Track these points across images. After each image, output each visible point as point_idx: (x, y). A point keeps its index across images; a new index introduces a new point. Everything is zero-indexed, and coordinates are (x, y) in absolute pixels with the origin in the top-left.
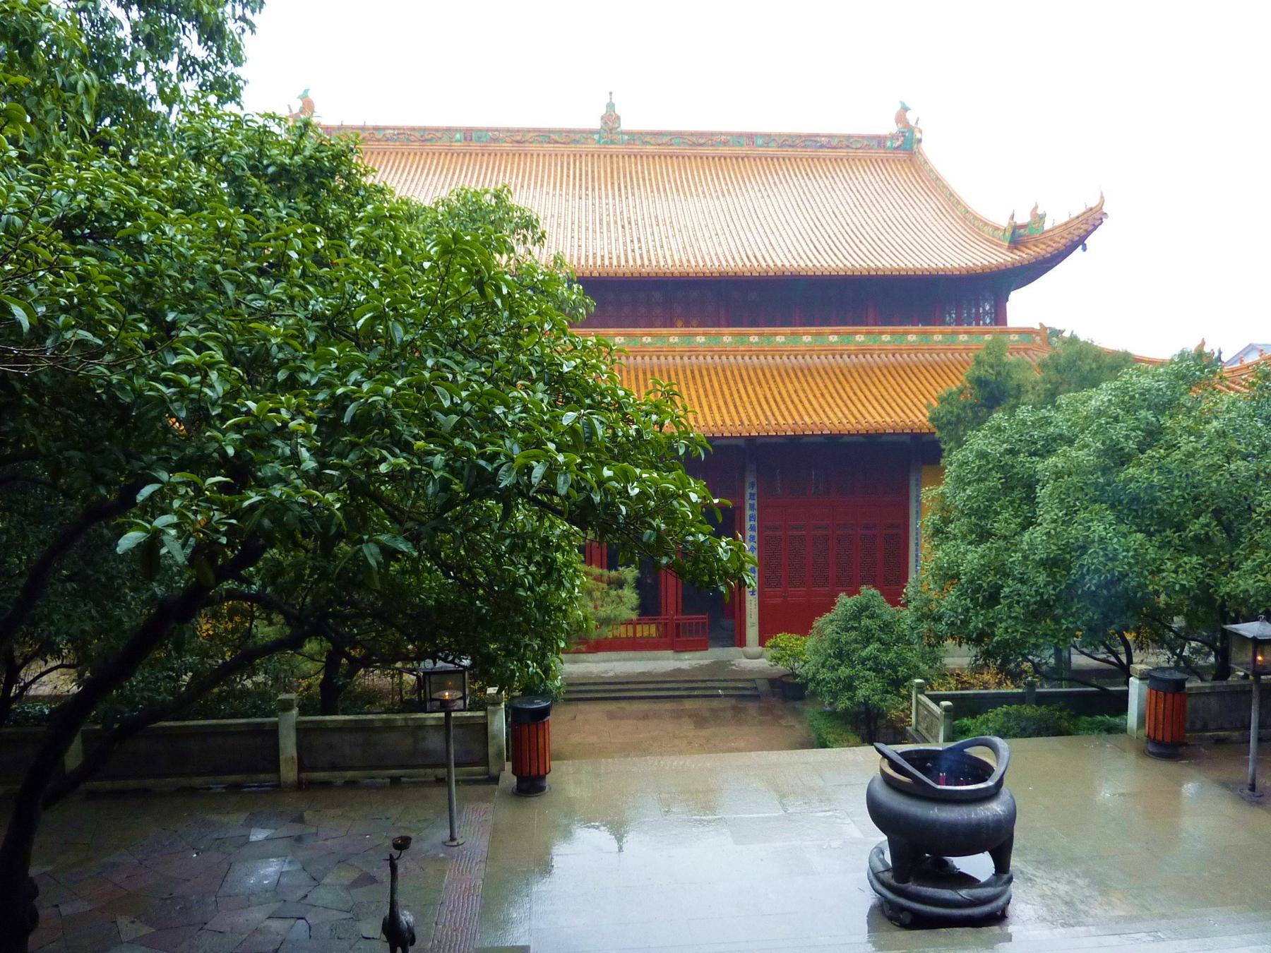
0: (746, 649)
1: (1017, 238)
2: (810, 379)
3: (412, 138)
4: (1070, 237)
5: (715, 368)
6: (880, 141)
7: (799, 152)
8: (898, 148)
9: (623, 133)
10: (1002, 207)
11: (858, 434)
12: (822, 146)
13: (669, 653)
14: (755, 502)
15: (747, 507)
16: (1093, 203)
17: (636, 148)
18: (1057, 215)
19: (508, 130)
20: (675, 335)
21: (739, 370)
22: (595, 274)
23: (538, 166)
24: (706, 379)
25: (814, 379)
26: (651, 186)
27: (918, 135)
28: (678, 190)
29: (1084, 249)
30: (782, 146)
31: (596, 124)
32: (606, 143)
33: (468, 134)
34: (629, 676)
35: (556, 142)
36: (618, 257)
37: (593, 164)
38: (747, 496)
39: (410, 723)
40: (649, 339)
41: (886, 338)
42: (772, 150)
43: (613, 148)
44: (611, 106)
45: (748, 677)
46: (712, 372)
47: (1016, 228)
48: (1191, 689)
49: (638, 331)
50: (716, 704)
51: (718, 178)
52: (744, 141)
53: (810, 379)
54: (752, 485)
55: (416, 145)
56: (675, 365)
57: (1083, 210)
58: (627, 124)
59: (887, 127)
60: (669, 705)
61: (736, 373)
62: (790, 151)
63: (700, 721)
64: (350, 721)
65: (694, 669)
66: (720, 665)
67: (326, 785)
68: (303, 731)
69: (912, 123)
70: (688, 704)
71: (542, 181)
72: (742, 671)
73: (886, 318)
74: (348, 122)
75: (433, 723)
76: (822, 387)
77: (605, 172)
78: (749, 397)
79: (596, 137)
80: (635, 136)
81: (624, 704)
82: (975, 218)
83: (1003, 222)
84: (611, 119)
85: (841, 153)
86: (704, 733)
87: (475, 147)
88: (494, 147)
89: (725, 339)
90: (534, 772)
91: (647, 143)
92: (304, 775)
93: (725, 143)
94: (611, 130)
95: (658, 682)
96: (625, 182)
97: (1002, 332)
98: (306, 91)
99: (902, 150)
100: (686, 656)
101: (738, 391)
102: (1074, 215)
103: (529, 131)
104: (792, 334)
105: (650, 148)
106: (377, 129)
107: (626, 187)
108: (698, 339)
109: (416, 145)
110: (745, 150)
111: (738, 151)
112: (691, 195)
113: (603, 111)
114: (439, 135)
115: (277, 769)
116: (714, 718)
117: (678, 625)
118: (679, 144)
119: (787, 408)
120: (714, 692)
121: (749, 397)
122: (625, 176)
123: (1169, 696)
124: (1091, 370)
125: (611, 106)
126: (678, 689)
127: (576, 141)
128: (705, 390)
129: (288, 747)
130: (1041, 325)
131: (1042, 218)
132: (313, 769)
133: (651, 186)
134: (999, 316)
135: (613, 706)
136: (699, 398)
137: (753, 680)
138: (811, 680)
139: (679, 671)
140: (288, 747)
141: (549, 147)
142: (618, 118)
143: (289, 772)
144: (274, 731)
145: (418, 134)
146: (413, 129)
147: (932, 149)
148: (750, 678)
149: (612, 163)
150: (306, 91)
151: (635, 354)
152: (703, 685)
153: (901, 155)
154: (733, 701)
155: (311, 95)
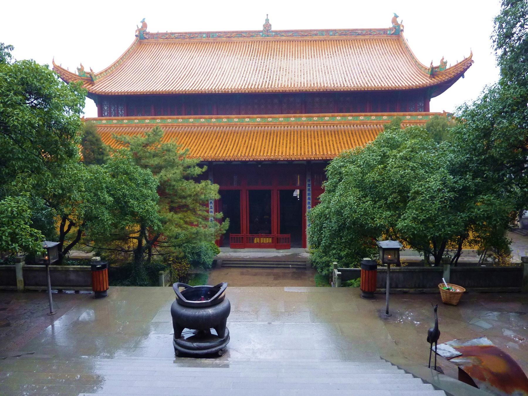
0: (306, 249)
1: (434, 72)
2: (337, 136)
3: (186, 37)
4: (456, 72)
5: (338, 132)
6: (385, 31)
7: (348, 37)
8: (392, 34)
9: (272, 32)
10: (428, 58)
11: (268, 161)
12: (358, 35)
13: (274, 250)
14: (310, 188)
15: (307, 190)
16: (467, 56)
17: (277, 38)
18: (452, 62)
19: (225, 32)
20: (282, 117)
21: (307, 132)
22: (247, 92)
23: (236, 47)
24: (292, 136)
25: (339, 136)
26: (282, 54)
27: (402, 28)
28: (292, 56)
29: (463, 78)
30: (340, 35)
31: (261, 28)
32: (265, 36)
33: (209, 34)
34: (256, 258)
35: (244, 37)
36: (304, 83)
37: (259, 46)
38: (307, 185)
39: (64, 269)
40: (271, 119)
41: (191, 120)
42: (336, 37)
43: (269, 38)
44: (267, 20)
45: (303, 260)
46: (296, 133)
47: (433, 68)
48: (379, 269)
49: (255, 116)
50: (287, 271)
51: (311, 50)
52: (324, 33)
53: (337, 136)
54: (309, 181)
55: (187, 40)
56: (304, 130)
57: (463, 59)
58: (274, 28)
59: (388, 25)
60: (240, 270)
61: (306, 133)
62: (344, 37)
63: (277, 277)
64: (42, 267)
65: (283, 256)
66: (295, 255)
67: (36, 291)
68: (24, 270)
69: (399, 23)
70: (276, 271)
71: (276, 54)
72: (303, 258)
73: (171, 112)
74: (160, 32)
75: (72, 269)
76: (341, 139)
77: (264, 48)
78: (308, 144)
79: (261, 34)
80: (278, 33)
81: (249, 270)
82: (419, 64)
83: (428, 66)
84: (267, 25)
85: (367, 37)
86: (276, 282)
87: (211, 40)
88: (219, 40)
89: (303, 119)
90: (102, 290)
91: (282, 35)
92: (26, 287)
93: (316, 35)
94: (267, 30)
95: (265, 261)
96: (271, 53)
97: (426, 115)
98: (144, 19)
99: (394, 35)
100: (281, 251)
101: (304, 141)
102: (459, 62)
103: (233, 32)
104: (332, 116)
105: (284, 38)
106: (172, 34)
107: (271, 55)
108: (291, 119)
109: (187, 40)
110: (325, 37)
111: (321, 38)
112: (298, 58)
113: (264, 22)
114: (196, 35)
115: (15, 284)
116: (284, 276)
117: (278, 238)
118: (296, 36)
119: (323, 148)
120: (287, 266)
121: (308, 144)
122: (271, 50)
123: (367, 272)
124: (440, 131)
125: (267, 20)
126: (273, 264)
127: (252, 36)
128: (290, 141)
129: (20, 276)
130: (444, 111)
131: (445, 63)
132: (29, 285)
133: (282, 54)
134: (426, 108)
135: (245, 270)
136: (287, 144)
137: (305, 262)
138: (314, 262)
139: (276, 257)
140: (20, 276)
141: (241, 39)
142: (270, 25)
143: (20, 285)
144: (13, 271)
145: (188, 35)
146: (186, 33)
147: (406, 35)
148: (304, 261)
149: (267, 45)
150: (144, 19)
151: (265, 125)
152: (283, 263)
153: (394, 37)
154: (295, 270)
155: (146, 21)
